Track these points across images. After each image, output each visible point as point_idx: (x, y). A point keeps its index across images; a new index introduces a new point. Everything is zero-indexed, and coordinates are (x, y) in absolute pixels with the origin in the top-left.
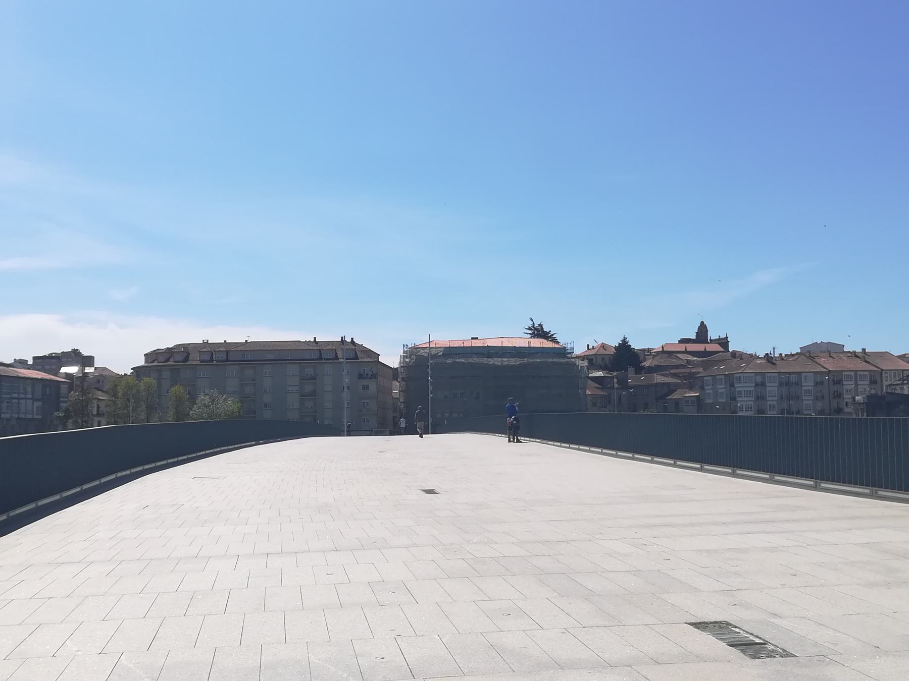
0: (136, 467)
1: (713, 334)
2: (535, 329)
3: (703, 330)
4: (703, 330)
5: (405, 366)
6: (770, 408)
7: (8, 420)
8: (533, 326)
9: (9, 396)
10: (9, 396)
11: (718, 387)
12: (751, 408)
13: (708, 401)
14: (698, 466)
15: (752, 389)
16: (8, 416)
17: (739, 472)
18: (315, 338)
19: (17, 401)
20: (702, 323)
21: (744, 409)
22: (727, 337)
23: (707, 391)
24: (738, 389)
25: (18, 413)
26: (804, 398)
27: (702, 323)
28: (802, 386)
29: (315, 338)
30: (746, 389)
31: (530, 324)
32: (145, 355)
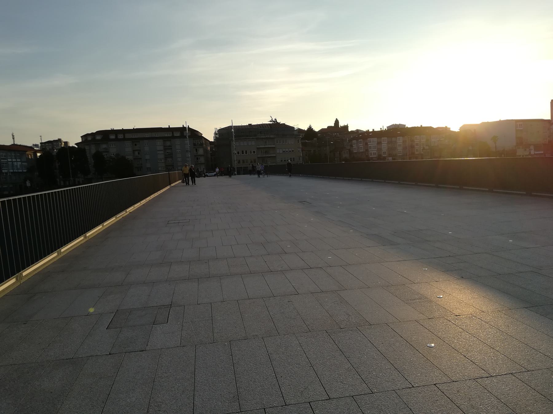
0: (24, 194)
1: (341, 124)
2: (273, 121)
3: (337, 122)
4: (337, 122)
5: (216, 139)
6: (416, 151)
7: (6, 173)
8: (272, 120)
9: (6, 160)
10: (6, 160)
11: (360, 145)
12: (376, 154)
13: (354, 152)
14: (334, 178)
15: (376, 145)
16: (6, 171)
17: (337, 178)
18: (169, 126)
19: (11, 163)
20: (337, 119)
21: (372, 154)
22: (348, 125)
23: (354, 147)
24: (369, 145)
25: (13, 169)
26: (398, 148)
27: (337, 119)
28: (382, 144)
29: (169, 126)
30: (373, 145)
31: (270, 119)
32: (81, 137)
